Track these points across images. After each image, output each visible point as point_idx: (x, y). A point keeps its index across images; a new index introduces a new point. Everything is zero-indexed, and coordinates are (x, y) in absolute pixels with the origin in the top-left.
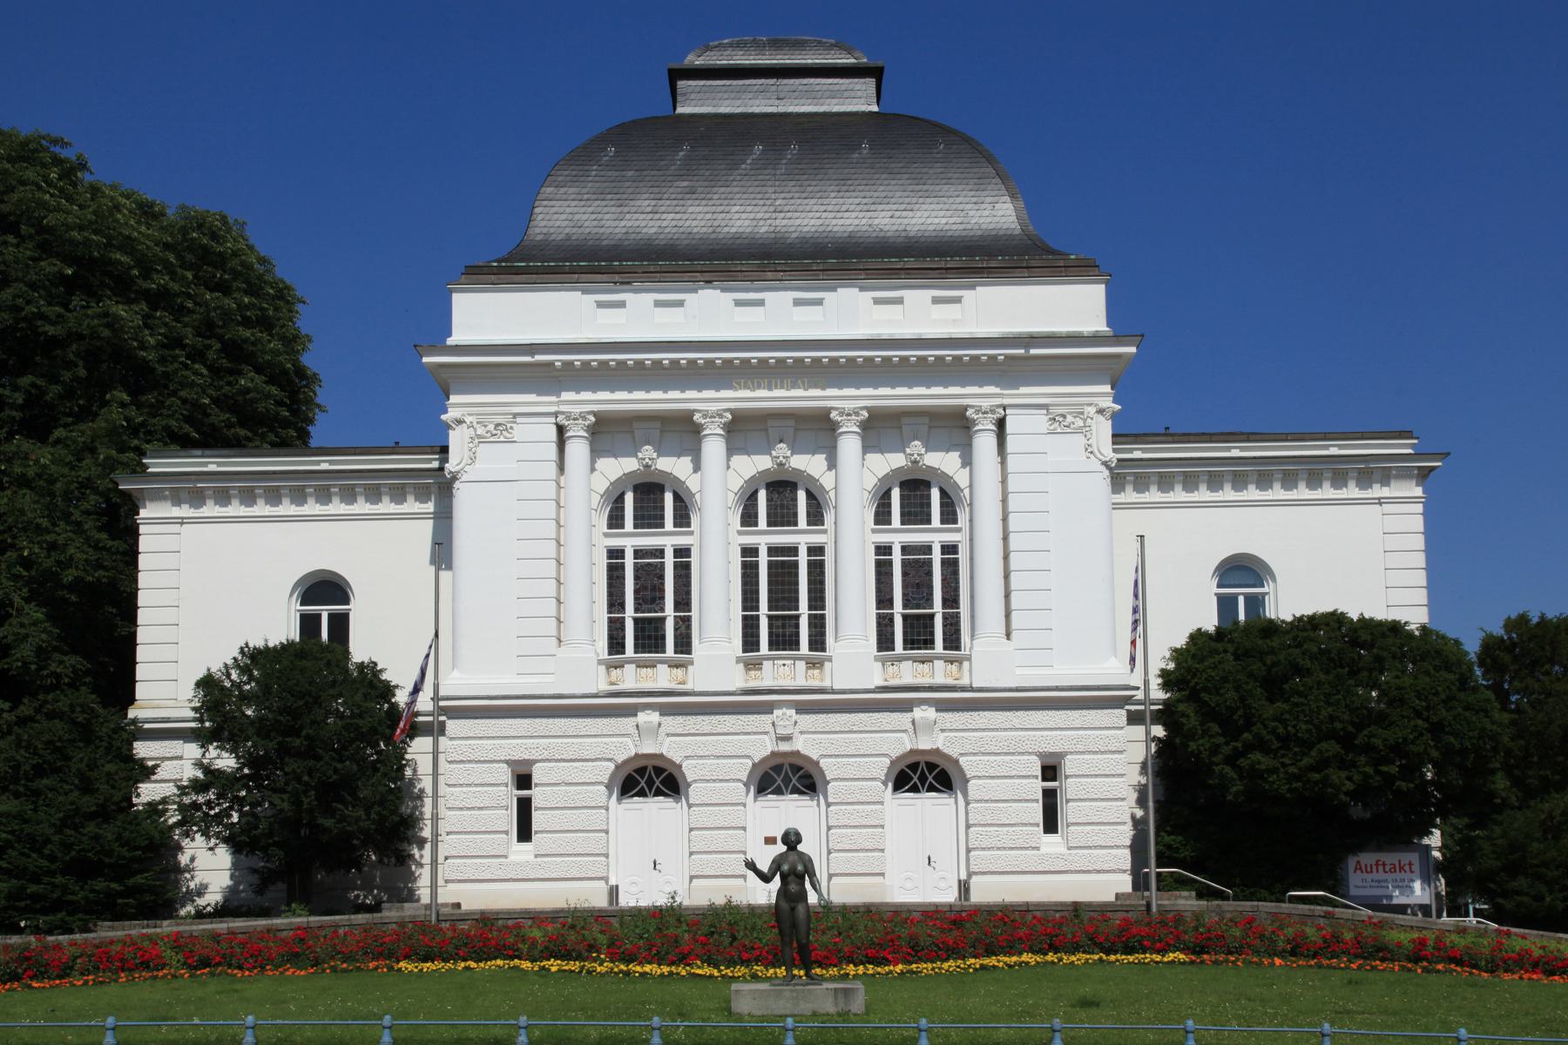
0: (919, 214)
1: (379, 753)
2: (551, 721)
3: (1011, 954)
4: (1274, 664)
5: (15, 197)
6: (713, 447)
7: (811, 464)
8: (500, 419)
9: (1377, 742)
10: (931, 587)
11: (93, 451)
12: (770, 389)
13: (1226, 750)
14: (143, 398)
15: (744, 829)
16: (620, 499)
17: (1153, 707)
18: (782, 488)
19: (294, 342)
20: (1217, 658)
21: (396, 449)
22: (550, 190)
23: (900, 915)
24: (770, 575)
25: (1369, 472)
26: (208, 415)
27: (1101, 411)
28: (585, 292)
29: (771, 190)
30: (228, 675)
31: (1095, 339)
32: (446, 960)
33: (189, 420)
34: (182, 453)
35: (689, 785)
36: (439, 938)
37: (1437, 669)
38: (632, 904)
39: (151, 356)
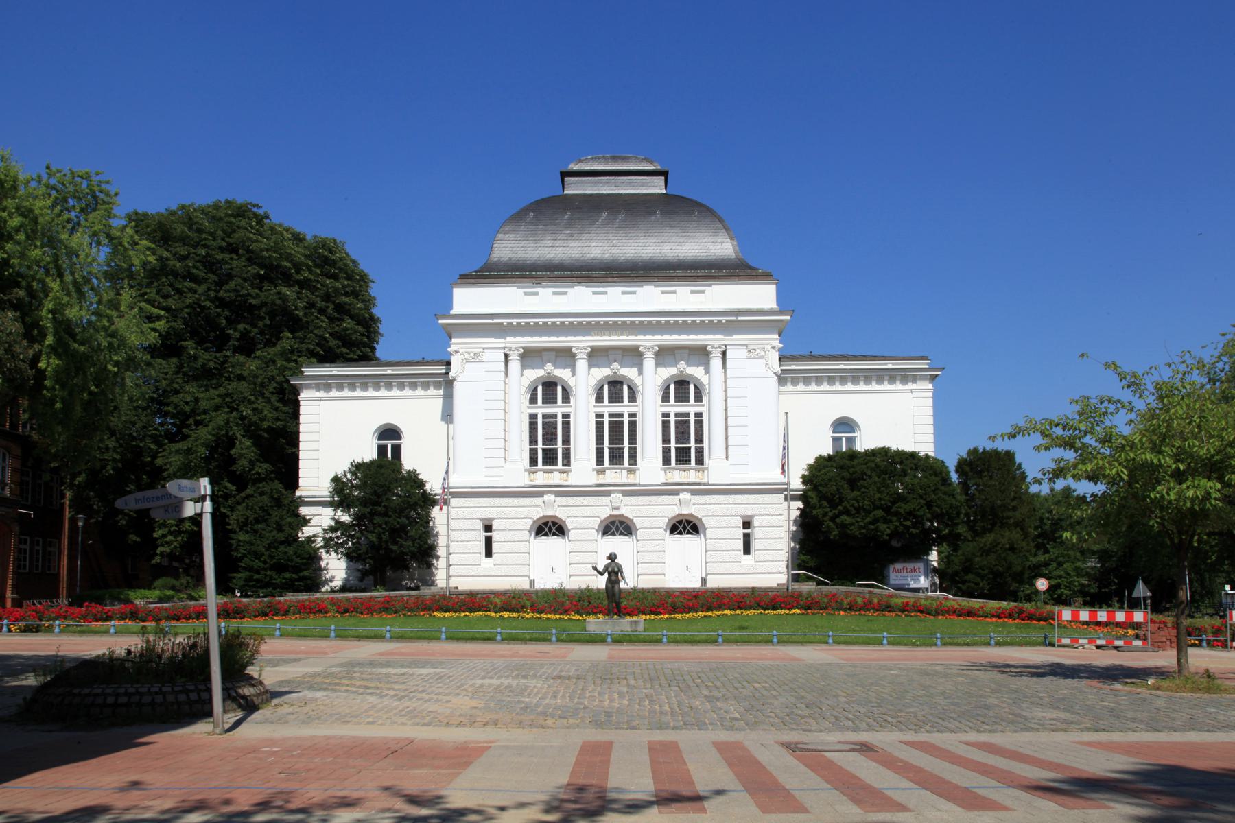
0: (684, 248)
1: (418, 514)
2: (502, 499)
3: (719, 610)
4: (854, 473)
5: (237, 235)
6: (582, 364)
7: (630, 373)
9: (901, 510)
10: (689, 434)
11: (274, 362)
12: (610, 336)
13: (830, 514)
14: (297, 335)
15: (596, 552)
16: (535, 389)
17: (792, 493)
18: (615, 384)
19: (369, 302)
20: (827, 469)
21: (422, 363)
22: (501, 235)
23: (670, 593)
24: (609, 427)
25: (907, 376)
26: (328, 342)
27: (773, 348)
28: (518, 287)
29: (611, 235)
30: (346, 476)
32: (455, 612)
33: (318, 345)
34: (320, 365)
35: (569, 531)
36: (452, 602)
37: (931, 475)
38: (542, 587)
39: (300, 314)
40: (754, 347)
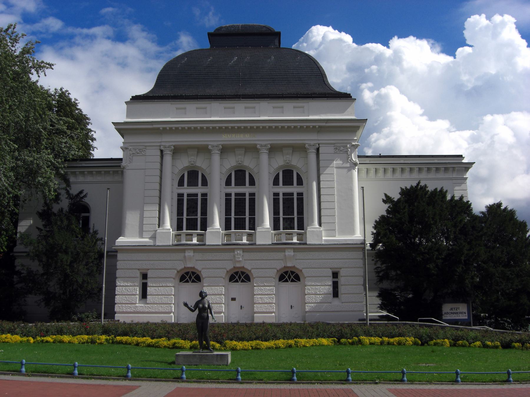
8: (141, 147)
40: (339, 145)
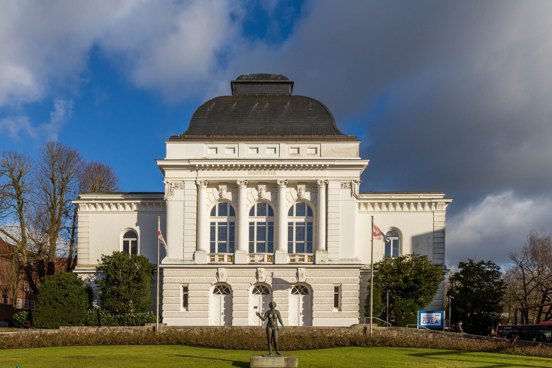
31: (166, 170)
